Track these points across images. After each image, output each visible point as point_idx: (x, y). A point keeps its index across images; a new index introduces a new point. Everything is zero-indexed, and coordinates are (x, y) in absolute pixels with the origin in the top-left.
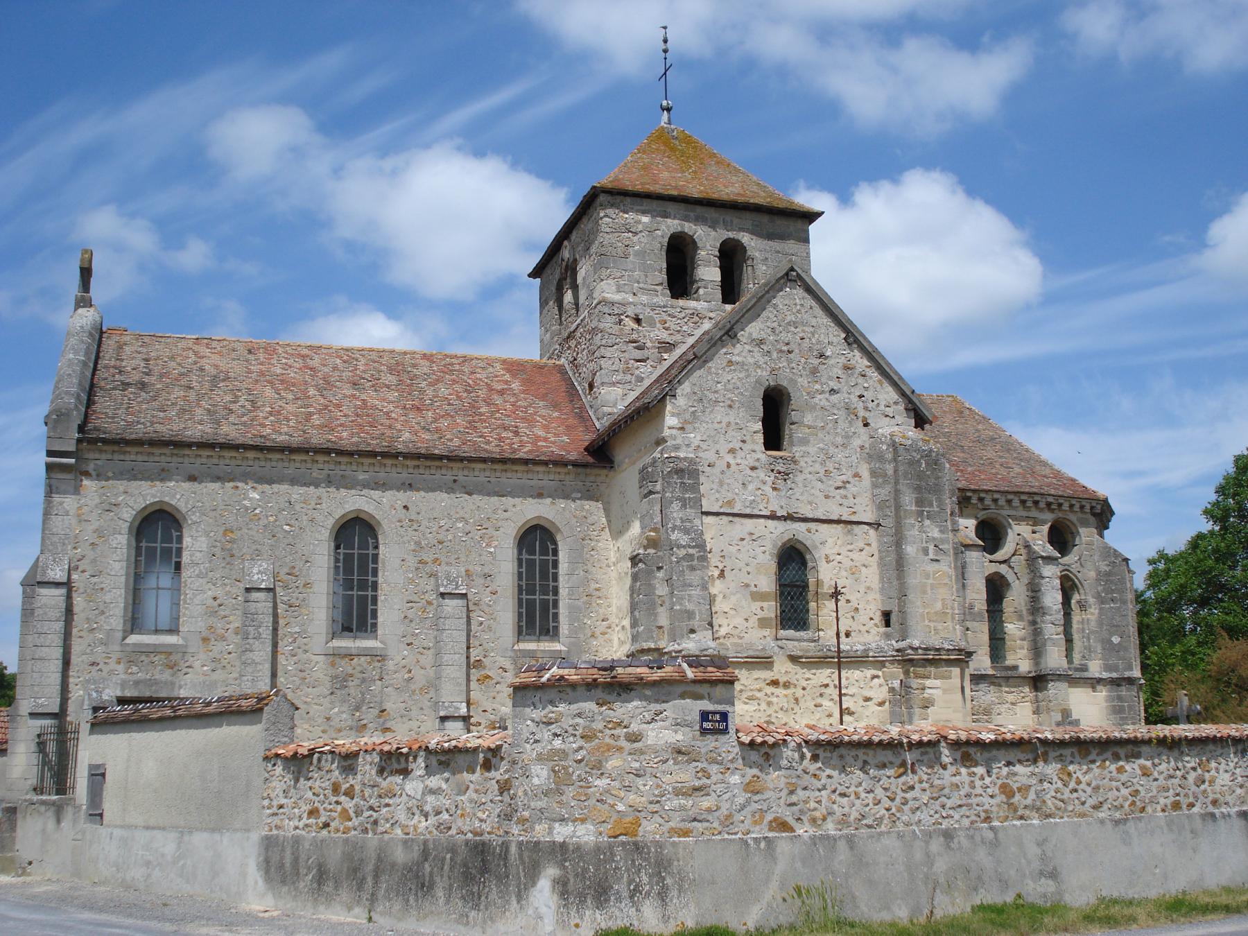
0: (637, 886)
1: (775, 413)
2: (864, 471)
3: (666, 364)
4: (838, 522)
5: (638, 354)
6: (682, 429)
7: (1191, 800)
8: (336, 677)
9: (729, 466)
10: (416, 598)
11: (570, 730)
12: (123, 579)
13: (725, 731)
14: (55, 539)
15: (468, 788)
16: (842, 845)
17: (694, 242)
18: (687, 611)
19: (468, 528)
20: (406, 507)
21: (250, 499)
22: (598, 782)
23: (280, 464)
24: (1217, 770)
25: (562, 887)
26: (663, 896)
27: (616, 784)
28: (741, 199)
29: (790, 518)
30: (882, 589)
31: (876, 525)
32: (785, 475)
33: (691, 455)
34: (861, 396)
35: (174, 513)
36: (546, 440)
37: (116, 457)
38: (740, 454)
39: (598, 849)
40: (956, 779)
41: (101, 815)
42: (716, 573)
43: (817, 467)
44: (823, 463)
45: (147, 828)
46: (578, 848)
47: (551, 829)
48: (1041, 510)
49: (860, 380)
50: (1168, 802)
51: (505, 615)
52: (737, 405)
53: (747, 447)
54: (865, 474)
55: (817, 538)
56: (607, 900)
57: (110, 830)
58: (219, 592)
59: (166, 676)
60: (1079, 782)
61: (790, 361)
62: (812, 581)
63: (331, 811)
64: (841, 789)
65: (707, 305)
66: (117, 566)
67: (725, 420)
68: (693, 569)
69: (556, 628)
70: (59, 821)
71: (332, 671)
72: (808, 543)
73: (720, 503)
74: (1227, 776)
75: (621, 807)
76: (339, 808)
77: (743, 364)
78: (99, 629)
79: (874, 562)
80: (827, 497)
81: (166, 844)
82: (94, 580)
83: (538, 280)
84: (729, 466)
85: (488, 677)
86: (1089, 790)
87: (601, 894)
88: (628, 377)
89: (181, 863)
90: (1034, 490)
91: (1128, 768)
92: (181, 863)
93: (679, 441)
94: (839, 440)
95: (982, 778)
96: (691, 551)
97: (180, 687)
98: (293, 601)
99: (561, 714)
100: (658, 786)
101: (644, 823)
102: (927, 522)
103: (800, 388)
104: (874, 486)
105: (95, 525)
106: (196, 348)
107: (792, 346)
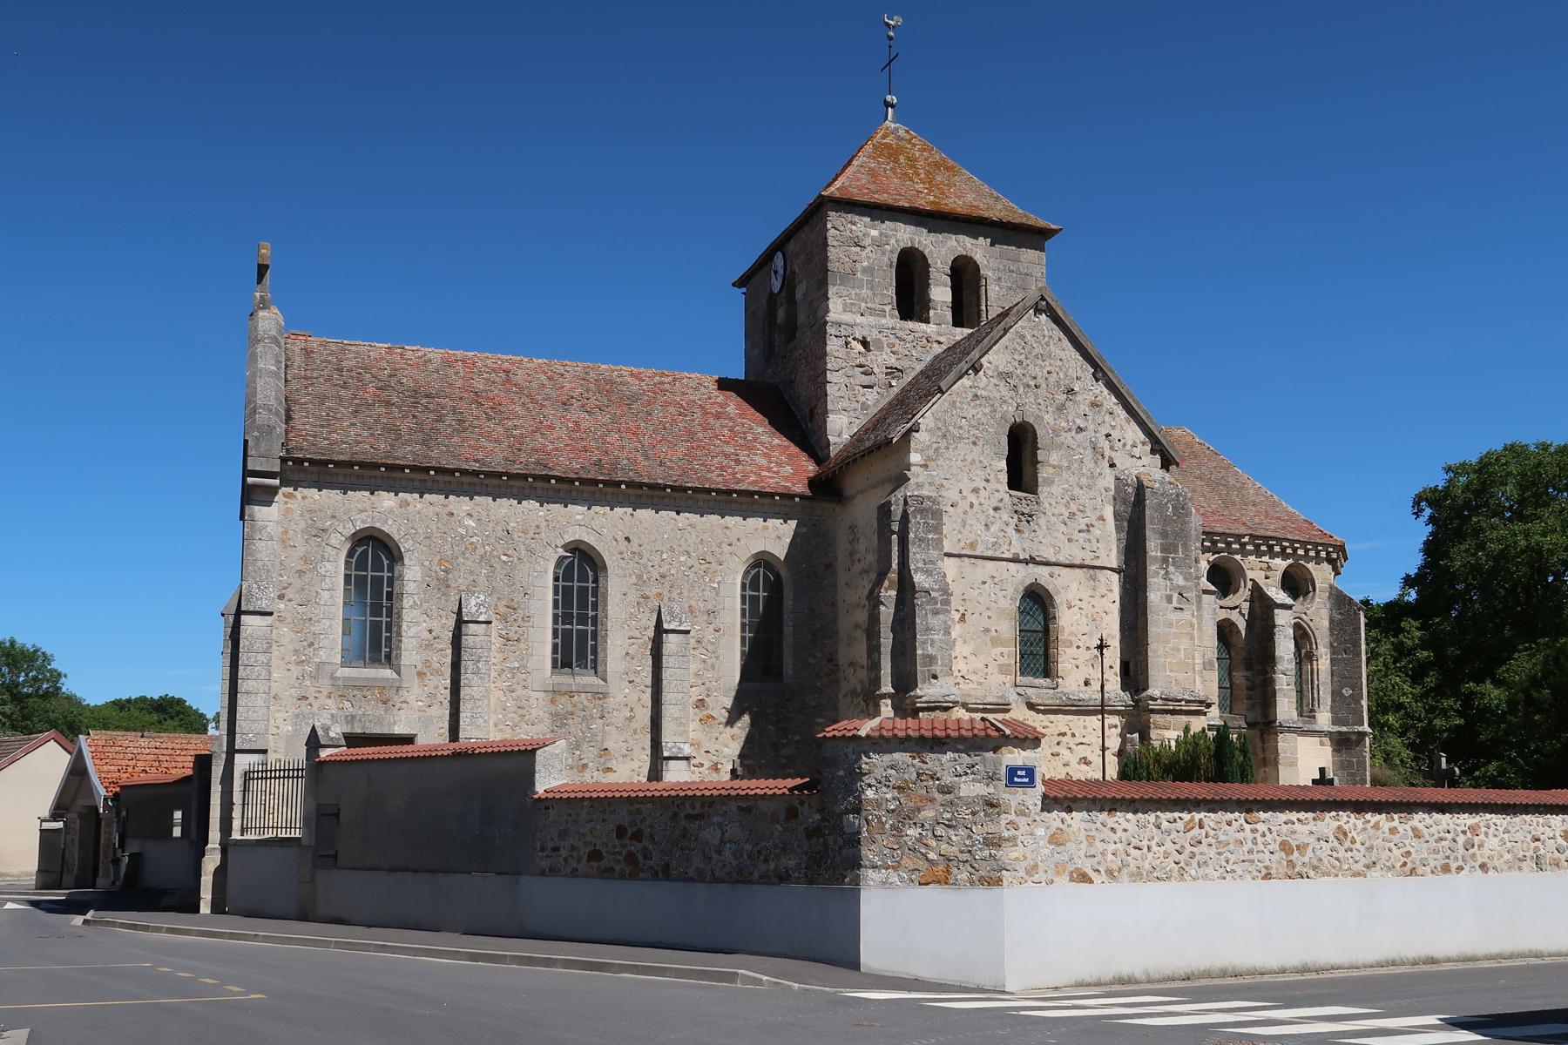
1: (1021, 457)
3: (896, 390)
4: (1081, 566)
5: (866, 380)
7: (1460, 863)
9: (972, 505)
10: (637, 634)
17: (925, 259)
18: (930, 656)
19: (690, 562)
20: (627, 539)
21: (466, 527)
24: (1486, 834)
28: (975, 213)
29: (1032, 561)
33: (934, 494)
34: (1108, 435)
35: (386, 540)
36: (769, 469)
40: (1240, 836)
41: (335, 857)
42: (957, 616)
44: (1067, 505)
49: (1108, 418)
50: (1439, 864)
52: (980, 443)
53: (990, 487)
55: (1058, 582)
58: (434, 625)
60: (1353, 841)
64: (1135, 842)
65: (939, 331)
68: (936, 613)
71: (553, 709)
72: (1050, 588)
73: (962, 544)
74: (1496, 840)
77: (987, 398)
80: (1070, 540)
84: (972, 505)
86: (1362, 849)
90: (1269, 534)
91: (1400, 829)
94: (1084, 481)
95: (1264, 835)
102: (1171, 569)
103: (1046, 423)
105: (301, 551)
106: (388, 357)
107: (1040, 381)
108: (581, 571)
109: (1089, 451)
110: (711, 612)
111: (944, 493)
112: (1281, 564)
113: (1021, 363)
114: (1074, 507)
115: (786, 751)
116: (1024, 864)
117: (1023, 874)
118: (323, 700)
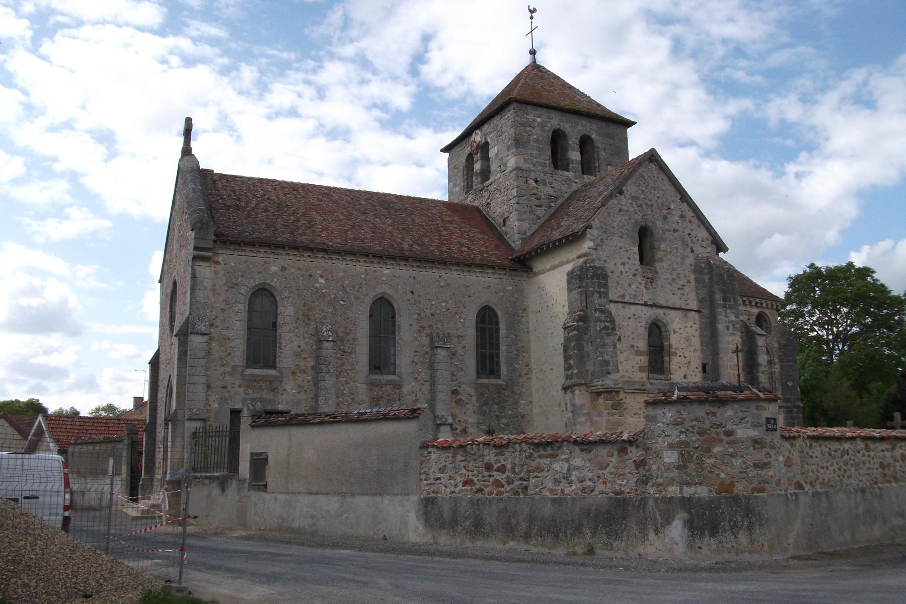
0: (735, 522)
2: (692, 277)
4: (680, 309)
6: (595, 249)
8: (373, 398)
9: (621, 273)
11: (690, 429)
12: (242, 332)
13: (775, 430)
14: (199, 305)
15: (608, 465)
16: (824, 497)
19: (448, 306)
20: (412, 292)
22: (708, 461)
23: (337, 262)
25: (690, 524)
26: (750, 528)
27: (719, 461)
29: (653, 306)
30: (702, 350)
31: (699, 312)
32: (652, 280)
34: (689, 234)
36: (487, 253)
37: (236, 253)
38: (627, 266)
39: (711, 501)
40: (863, 459)
41: (265, 486)
43: (668, 276)
44: (671, 274)
45: (310, 494)
46: (700, 499)
47: (681, 489)
48: (751, 306)
49: (689, 224)
51: (471, 362)
52: (625, 236)
53: (631, 261)
54: (693, 281)
56: (717, 532)
57: (274, 495)
58: (302, 343)
59: (268, 396)
61: (652, 211)
62: (665, 343)
63: (484, 481)
66: (238, 323)
67: (619, 245)
68: (608, 335)
69: (499, 371)
70: (223, 490)
75: (723, 475)
76: (492, 479)
78: (227, 364)
79: (697, 333)
81: (332, 504)
82: (224, 332)
83: (447, 155)
84: (621, 273)
85: (461, 400)
87: (713, 529)
88: (532, 216)
89: (345, 516)
92: (345, 516)
93: (594, 257)
96: (608, 324)
97: (279, 403)
98: (346, 349)
99: (684, 419)
100: (745, 463)
101: (737, 484)
102: (728, 311)
104: (697, 288)
108: (383, 313)
109: (680, 243)
110: (460, 337)
111: (606, 265)
112: (755, 311)
113: (643, 191)
114: (674, 276)
115: (504, 420)
116: (775, 479)
117: (774, 485)
118: (237, 389)
